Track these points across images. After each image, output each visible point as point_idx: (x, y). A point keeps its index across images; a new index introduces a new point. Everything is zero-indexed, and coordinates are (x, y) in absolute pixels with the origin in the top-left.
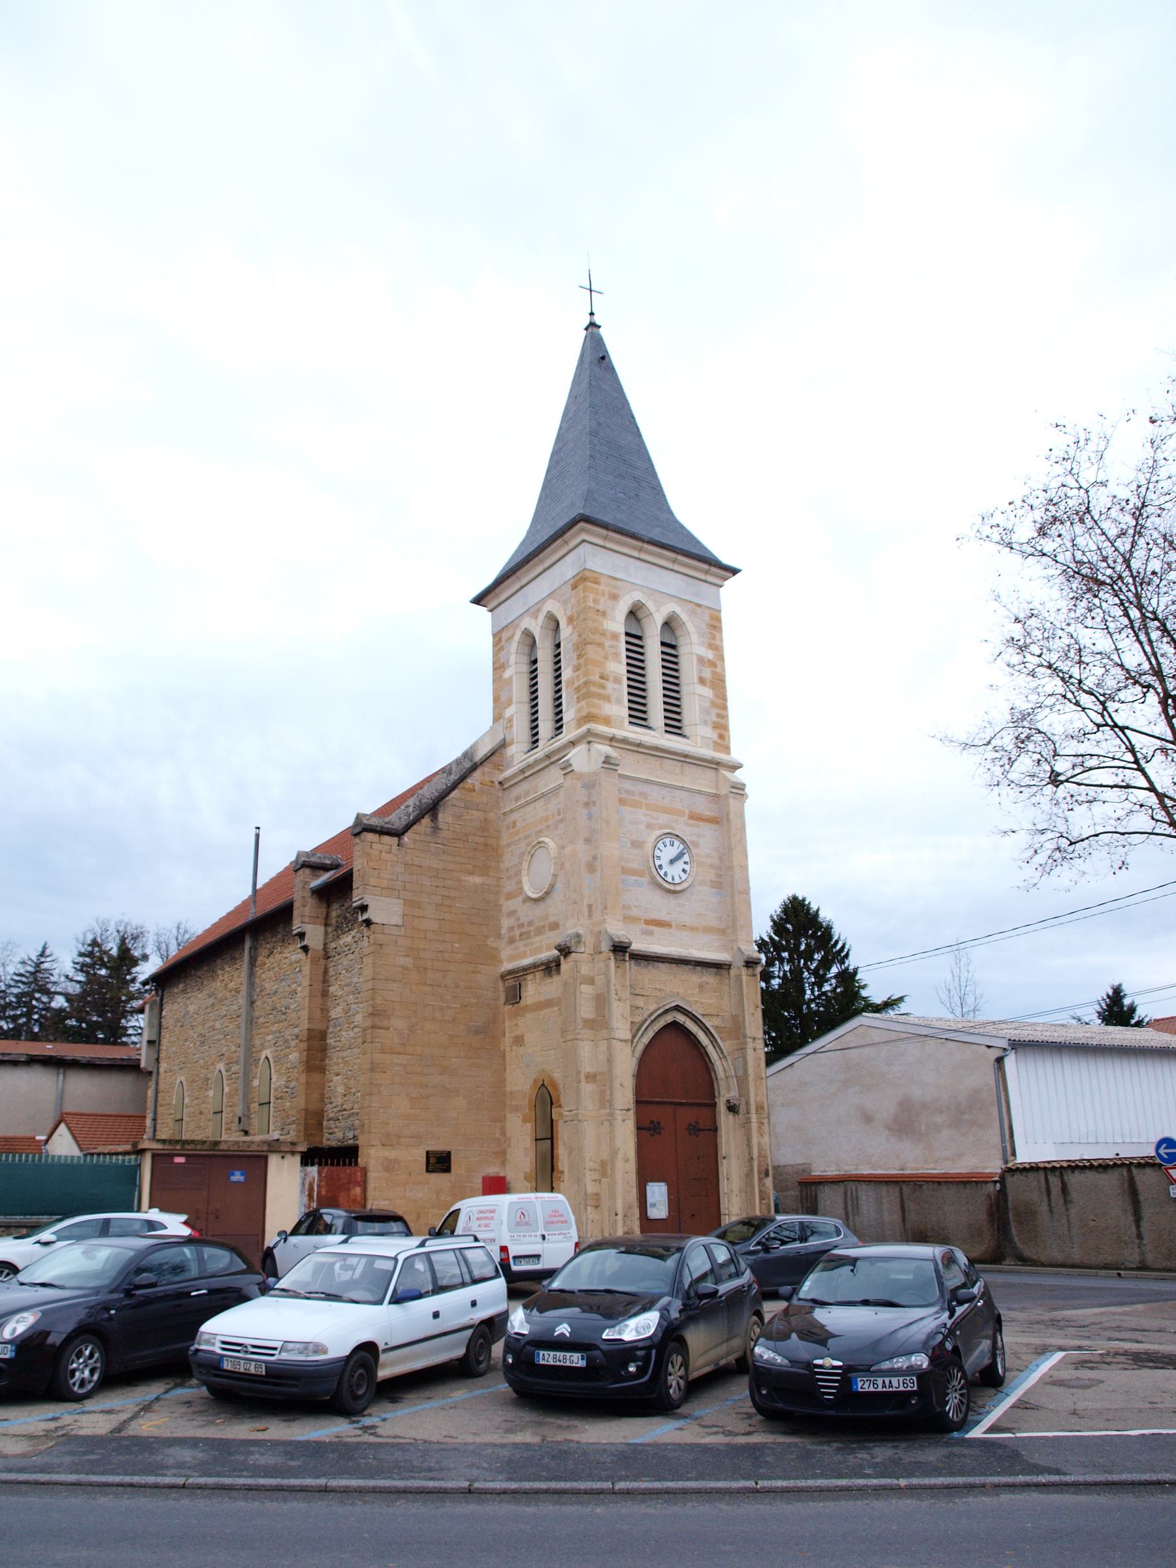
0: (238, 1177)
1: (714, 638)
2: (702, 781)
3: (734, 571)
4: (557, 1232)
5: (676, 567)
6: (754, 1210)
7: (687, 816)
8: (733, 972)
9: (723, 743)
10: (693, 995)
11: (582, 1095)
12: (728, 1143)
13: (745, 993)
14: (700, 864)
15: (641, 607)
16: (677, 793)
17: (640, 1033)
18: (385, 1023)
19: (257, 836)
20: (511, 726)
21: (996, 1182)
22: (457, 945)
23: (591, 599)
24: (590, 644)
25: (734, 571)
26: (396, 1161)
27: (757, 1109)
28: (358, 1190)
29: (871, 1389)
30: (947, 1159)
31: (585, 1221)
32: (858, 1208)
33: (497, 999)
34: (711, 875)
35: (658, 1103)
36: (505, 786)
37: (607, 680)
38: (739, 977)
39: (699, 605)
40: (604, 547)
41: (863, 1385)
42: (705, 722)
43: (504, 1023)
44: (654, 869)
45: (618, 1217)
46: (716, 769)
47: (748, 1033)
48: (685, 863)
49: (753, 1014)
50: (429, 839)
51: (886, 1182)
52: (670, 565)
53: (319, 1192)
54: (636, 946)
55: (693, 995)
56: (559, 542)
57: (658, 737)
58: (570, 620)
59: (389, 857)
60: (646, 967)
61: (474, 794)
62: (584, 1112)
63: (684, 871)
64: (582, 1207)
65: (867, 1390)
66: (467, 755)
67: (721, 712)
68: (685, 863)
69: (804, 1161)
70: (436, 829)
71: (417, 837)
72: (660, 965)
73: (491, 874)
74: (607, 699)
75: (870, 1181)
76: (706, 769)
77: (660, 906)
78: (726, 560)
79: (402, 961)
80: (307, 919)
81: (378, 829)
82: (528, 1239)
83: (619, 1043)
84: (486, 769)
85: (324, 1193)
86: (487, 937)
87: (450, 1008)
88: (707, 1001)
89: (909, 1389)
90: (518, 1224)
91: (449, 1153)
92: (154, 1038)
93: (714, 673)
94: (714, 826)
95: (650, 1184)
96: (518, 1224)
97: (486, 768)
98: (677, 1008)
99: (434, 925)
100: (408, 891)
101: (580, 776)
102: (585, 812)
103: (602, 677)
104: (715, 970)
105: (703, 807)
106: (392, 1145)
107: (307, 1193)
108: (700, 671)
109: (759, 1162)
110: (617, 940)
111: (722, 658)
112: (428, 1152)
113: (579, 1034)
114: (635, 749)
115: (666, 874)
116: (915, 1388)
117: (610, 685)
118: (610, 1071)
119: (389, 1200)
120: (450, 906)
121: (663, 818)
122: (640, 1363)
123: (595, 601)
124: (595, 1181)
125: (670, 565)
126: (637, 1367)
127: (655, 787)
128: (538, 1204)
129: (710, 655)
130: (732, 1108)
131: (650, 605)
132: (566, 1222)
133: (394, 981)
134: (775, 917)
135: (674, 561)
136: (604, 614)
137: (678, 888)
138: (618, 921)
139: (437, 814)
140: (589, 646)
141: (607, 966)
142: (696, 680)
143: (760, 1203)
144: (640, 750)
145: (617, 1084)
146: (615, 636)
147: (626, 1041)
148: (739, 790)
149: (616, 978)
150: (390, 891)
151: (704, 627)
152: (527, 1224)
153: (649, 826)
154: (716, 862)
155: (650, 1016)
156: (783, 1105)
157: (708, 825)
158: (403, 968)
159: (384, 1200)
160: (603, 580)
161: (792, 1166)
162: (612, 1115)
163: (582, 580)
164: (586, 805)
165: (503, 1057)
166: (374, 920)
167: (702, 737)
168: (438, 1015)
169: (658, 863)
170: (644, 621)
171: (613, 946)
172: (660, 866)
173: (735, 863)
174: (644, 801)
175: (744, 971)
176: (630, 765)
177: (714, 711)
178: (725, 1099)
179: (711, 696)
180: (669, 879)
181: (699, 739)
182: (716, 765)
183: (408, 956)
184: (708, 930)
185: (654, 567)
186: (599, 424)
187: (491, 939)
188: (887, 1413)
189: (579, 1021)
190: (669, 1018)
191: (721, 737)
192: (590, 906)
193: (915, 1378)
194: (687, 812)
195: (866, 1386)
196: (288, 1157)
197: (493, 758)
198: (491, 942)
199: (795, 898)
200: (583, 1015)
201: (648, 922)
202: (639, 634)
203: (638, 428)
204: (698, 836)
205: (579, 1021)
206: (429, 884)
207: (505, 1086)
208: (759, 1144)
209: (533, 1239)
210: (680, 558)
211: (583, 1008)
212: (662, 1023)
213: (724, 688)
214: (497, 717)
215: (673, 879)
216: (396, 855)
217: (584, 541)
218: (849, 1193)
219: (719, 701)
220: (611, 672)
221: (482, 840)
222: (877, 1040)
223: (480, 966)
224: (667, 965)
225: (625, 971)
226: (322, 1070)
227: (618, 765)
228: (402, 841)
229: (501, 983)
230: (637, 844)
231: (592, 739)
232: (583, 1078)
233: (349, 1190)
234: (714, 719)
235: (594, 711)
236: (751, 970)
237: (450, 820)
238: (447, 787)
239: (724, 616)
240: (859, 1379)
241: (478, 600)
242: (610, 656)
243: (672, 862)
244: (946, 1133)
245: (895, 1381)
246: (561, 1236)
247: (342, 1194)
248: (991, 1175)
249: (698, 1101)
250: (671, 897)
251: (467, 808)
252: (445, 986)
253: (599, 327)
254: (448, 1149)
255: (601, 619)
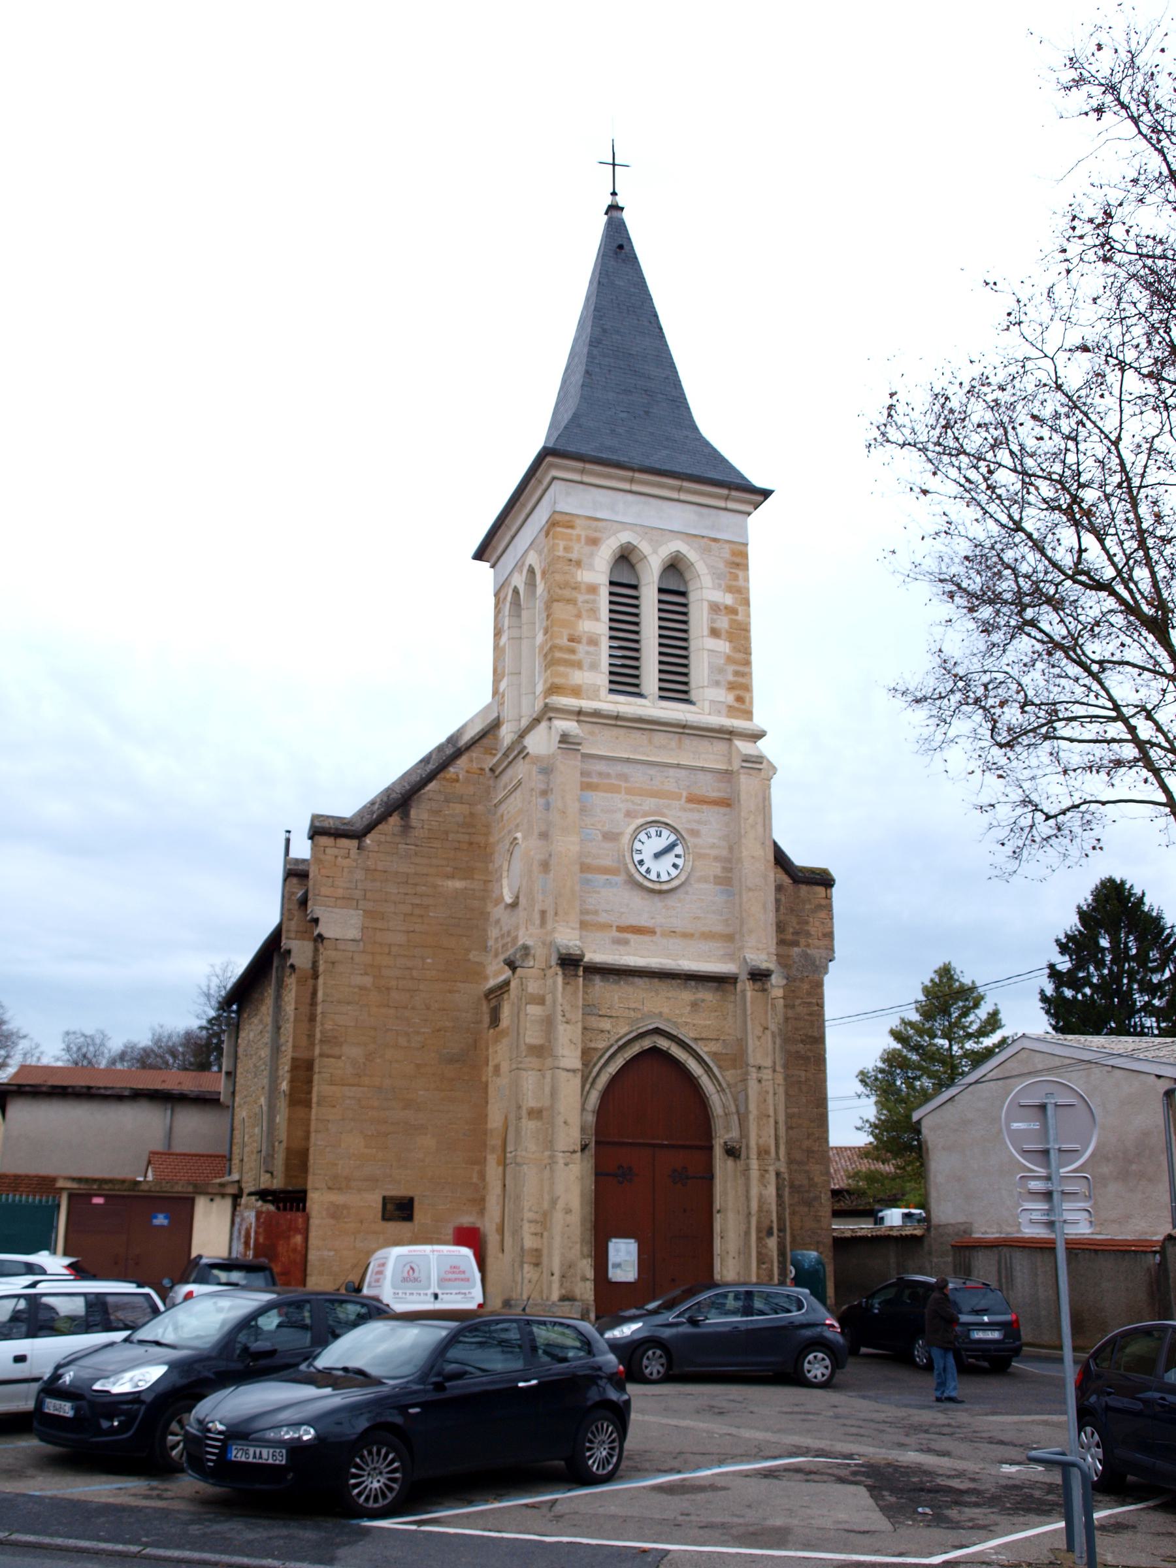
0: (161, 1220)
1: (736, 578)
2: (710, 756)
3: (766, 494)
4: (454, 1291)
5: (683, 497)
6: (749, 1275)
7: (684, 799)
8: (739, 986)
9: (743, 707)
10: (682, 1015)
11: (523, 1133)
12: (725, 1193)
13: (749, 1012)
14: (699, 856)
15: (633, 550)
16: (672, 772)
17: (602, 1061)
18: (336, 1051)
19: (288, 841)
20: (504, 703)
21: (1155, 1252)
22: (429, 961)
23: (561, 548)
24: (558, 601)
25: (766, 494)
26: (345, 1207)
27: (759, 1154)
28: (298, 1239)
29: (243, 1459)
30: (1114, 1221)
31: (520, 1280)
32: (1012, 1280)
33: (480, 1022)
34: (716, 869)
35: (631, 1144)
36: (497, 773)
37: (579, 642)
38: (743, 991)
39: (715, 540)
40: (582, 483)
41: (238, 1454)
42: (717, 683)
43: (487, 1049)
44: (631, 867)
45: (554, 1277)
46: (730, 740)
47: (751, 1061)
48: (677, 856)
49: (759, 1038)
50: (398, 839)
51: (1041, 1248)
52: (675, 495)
53: (256, 1240)
54: (595, 956)
55: (682, 1015)
56: (533, 481)
57: (651, 707)
58: (544, 573)
59: (346, 863)
60: (617, 982)
61: (457, 785)
62: (524, 1153)
63: (675, 866)
64: (516, 1265)
65: (239, 1459)
66: (452, 740)
67: (741, 669)
68: (677, 856)
69: (961, 1218)
70: (406, 828)
71: (383, 838)
72: (637, 980)
73: (476, 876)
74: (578, 665)
75: (1024, 1247)
76: (715, 741)
77: (640, 910)
78: (759, 482)
79: (358, 980)
80: (292, 935)
81: (332, 831)
82: (415, 1298)
83: (564, 1074)
84: (474, 755)
85: (261, 1240)
86: (468, 951)
87: (418, 1033)
88: (702, 1022)
89: (277, 1462)
90: (404, 1280)
91: (411, 1200)
92: (231, 1069)
93: (732, 621)
94: (723, 810)
95: (614, 1240)
96: (404, 1280)
97: (475, 753)
98: (657, 1031)
99: (401, 938)
100: (369, 900)
101: (537, 759)
102: (541, 801)
103: (571, 640)
104: (715, 984)
105: (709, 787)
106: (339, 1189)
107: (243, 1240)
108: (713, 621)
109: (759, 1217)
110: (564, 951)
111: (746, 602)
112: (384, 1198)
113: (521, 1062)
114: (613, 722)
115: (648, 871)
116: (284, 1462)
117: (582, 649)
118: (552, 1107)
119: (335, 1250)
120: (422, 916)
121: (650, 803)
122: (123, 1418)
123: (566, 549)
124: (536, 1234)
125: (675, 495)
126: (120, 1422)
127: (639, 766)
128: (433, 1260)
129: (728, 599)
130: (732, 1152)
131: (644, 547)
132: (468, 1280)
133: (349, 1003)
134: (1085, 908)
135: (680, 489)
136: (578, 564)
137: (665, 887)
138: (573, 929)
139: (409, 810)
140: (555, 604)
141: (555, 983)
142: (706, 632)
143: (758, 1268)
144: (619, 723)
145: (560, 1120)
146: (593, 589)
147: (574, 1071)
148: (757, 765)
149: (563, 997)
150: (347, 900)
151: (721, 565)
152: (416, 1280)
153: (629, 814)
154: (724, 853)
155: (617, 1041)
156: (943, 1148)
157: (716, 808)
158: (361, 988)
159: (329, 1250)
160: (578, 522)
161: (951, 1225)
162: (552, 1157)
163: (555, 523)
164: (544, 793)
165: (486, 1085)
166: (326, 935)
167: (711, 701)
168: (402, 1041)
169: (637, 858)
170: (639, 567)
171: (559, 959)
172: (641, 862)
173: (745, 853)
174: (623, 784)
175: (749, 986)
176: (602, 743)
177: (731, 668)
178: (722, 1141)
179: (727, 651)
180: (653, 876)
181: (707, 704)
182: (728, 735)
183: (366, 974)
184: (708, 936)
185: (652, 500)
186: (604, 331)
187: (474, 952)
188: (258, 1486)
189: (523, 1048)
190: (647, 1043)
191: (739, 699)
192: (543, 913)
193: (284, 1451)
194: (685, 794)
195: (239, 1455)
196: (218, 1200)
197: (485, 741)
198: (474, 956)
199: (1111, 880)
200: (529, 1040)
201: (620, 929)
202: (633, 582)
203: (661, 329)
204: (699, 822)
205: (523, 1048)
206: (396, 891)
207: (486, 1123)
208: (761, 1197)
209: (422, 1298)
210: (686, 484)
211: (528, 1033)
212: (636, 1049)
213: (747, 639)
214: (495, 692)
215: (659, 875)
216: (355, 860)
217: (554, 478)
218: (1003, 1261)
219: (740, 656)
220: (585, 632)
221: (467, 837)
222: (1040, 1067)
223: (459, 984)
224: (646, 980)
225: (577, 988)
226: (308, 1104)
227: (579, 744)
228: (364, 844)
229: (484, 1002)
230: (611, 837)
231: (552, 715)
232: (524, 1113)
233: (288, 1238)
234: (731, 678)
235: (559, 681)
236: (759, 984)
237: (425, 816)
238: (422, 779)
239: (752, 551)
240: (234, 1447)
241: (479, 555)
242: (584, 614)
243: (657, 855)
244: (1113, 1188)
245: (265, 1452)
246: (459, 1297)
247: (281, 1242)
248: (1152, 1243)
249: (688, 1143)
250: (656, 898)
251: (447, 801)
252: (413, 1008)
253: (622, 209)
254: (410, 1194)
255: (574, 569)
